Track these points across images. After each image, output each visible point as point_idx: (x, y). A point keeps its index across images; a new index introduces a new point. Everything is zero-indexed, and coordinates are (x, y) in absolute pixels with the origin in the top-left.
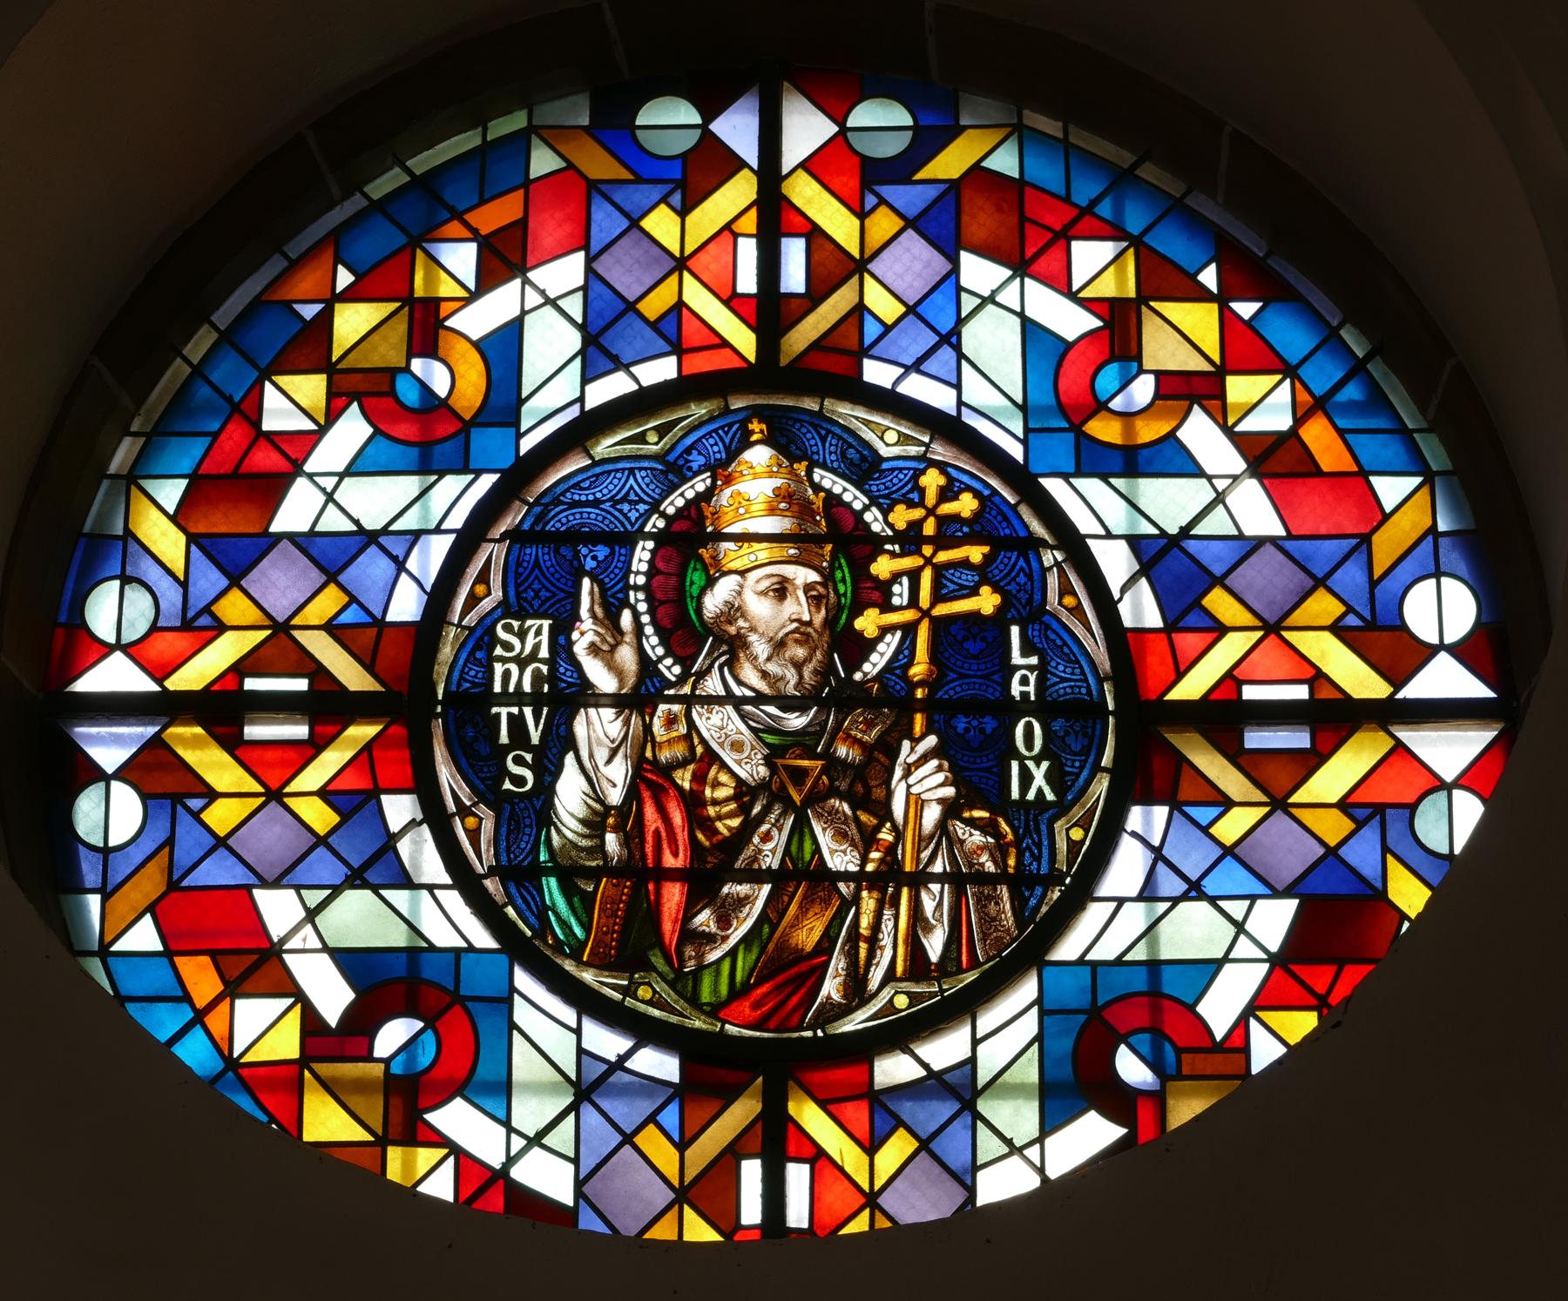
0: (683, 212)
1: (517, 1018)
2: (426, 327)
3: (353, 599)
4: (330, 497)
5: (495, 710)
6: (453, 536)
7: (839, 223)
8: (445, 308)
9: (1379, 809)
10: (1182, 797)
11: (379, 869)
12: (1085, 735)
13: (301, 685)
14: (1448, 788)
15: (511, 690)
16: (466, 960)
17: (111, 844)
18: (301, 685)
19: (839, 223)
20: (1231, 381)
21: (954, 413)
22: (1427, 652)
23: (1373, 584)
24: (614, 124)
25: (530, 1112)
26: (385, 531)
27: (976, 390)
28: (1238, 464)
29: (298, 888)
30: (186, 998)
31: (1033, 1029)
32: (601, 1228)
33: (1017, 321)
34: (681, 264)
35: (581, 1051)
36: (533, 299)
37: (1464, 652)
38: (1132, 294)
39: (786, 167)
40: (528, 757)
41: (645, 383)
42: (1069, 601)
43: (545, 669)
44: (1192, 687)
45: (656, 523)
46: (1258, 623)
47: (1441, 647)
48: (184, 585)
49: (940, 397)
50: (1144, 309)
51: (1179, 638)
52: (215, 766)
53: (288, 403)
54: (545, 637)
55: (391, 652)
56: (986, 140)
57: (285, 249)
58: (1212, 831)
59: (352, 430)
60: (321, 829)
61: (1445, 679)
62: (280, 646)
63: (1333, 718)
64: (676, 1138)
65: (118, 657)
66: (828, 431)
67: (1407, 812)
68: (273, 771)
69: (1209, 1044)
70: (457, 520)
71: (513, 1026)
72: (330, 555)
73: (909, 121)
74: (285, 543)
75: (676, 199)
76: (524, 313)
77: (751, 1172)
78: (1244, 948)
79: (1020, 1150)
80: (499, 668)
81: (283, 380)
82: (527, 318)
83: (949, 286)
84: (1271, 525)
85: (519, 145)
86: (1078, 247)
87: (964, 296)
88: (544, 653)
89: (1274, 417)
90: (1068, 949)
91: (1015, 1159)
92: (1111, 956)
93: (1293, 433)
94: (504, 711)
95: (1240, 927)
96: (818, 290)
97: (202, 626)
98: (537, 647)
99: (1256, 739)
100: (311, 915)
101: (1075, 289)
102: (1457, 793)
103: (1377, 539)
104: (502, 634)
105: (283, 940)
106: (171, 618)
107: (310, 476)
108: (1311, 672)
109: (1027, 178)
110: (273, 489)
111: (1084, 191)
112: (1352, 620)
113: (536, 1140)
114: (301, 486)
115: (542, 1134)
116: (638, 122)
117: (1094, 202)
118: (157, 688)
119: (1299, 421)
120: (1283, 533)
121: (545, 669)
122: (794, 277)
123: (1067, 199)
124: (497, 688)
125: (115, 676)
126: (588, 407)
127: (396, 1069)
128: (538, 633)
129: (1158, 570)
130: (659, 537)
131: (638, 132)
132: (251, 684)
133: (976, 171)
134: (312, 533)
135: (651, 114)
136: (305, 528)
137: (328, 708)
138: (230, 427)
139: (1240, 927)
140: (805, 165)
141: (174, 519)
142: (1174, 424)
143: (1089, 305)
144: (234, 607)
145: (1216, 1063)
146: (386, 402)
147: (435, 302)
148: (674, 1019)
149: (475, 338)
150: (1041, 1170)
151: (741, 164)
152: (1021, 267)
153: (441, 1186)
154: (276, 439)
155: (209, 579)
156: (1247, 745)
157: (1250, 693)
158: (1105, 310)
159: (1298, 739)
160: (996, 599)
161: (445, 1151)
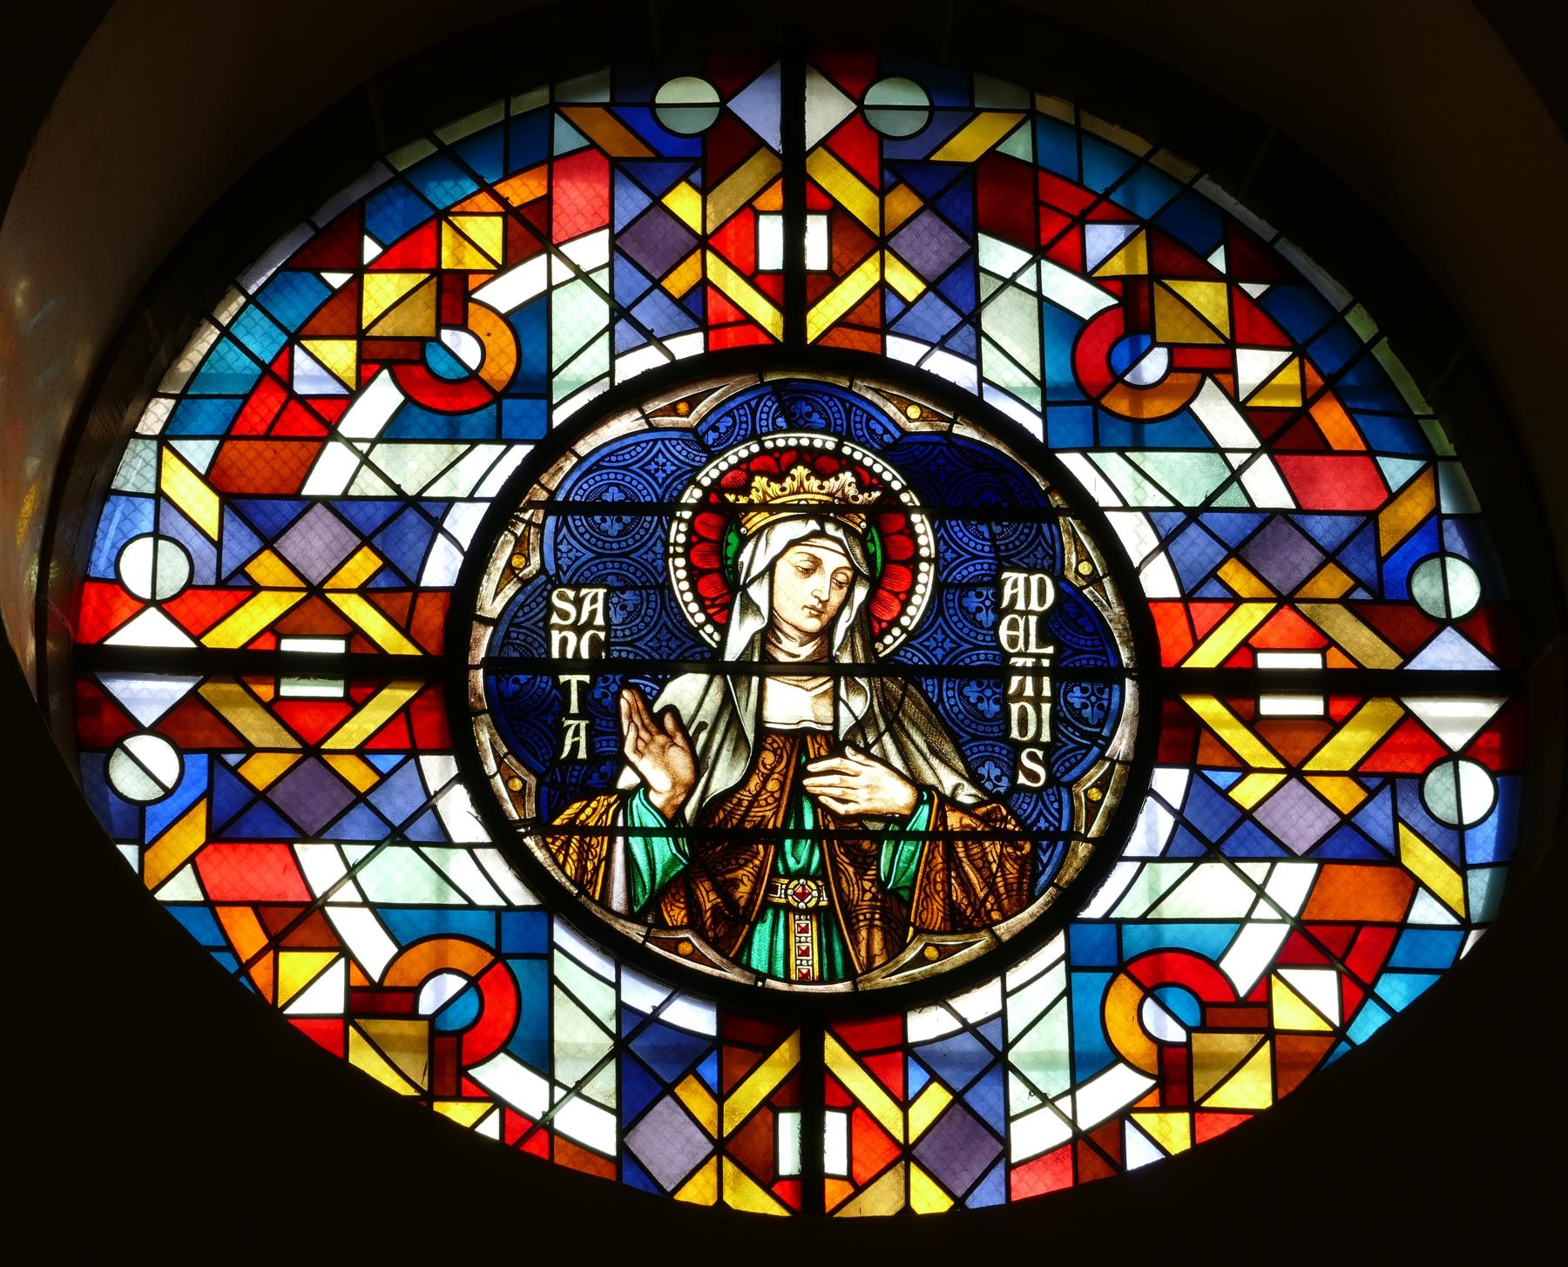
0: (704, 190)
1: (558, 972)
2: (453, 297)
5: (563, 678)
6: (487, 505)
7: (857, 199)
8: (473, 281)
9: (1390, 779)
10: (1200, 761)
12: (1101, 707)
19: (857, 199)
22: (1432, 626)
24: (634, 104)
28: (1250, 439)
33: (1033, 301)
34: (703, 242)
36: (561, 272)
40: (1040, 754)
41: (679, 357)
42: (682, 407)
43: (602, 635)
44: (1209, 655)
45: (692, 495)
46: (1271, 594)
48: (218, 545)
50: (1156, 286)
51: (1196, 608)
52: (253, 724)
53: (1310, 1000)
54: (600, 605)
55: (431, 616)
56: (1002, 124)
57: (313, 219)
60: (362, 787)
61: (149, 697)
62: (1293, 749)
63: (1347, 687)
64: (715, 1089)
65: (152, 612)
66: (852, 405)
67: (1416, 782)
69: (1232, 999)
71: (553, 980)
73: (925, 102)
74: (319, 508)
76: (551, 288)
77: (789, 1125)
78: (1263, 910)
80: (556, 636)
82: (555, 294)
84: (1283, 500)
85: (542, 121)
87: (983, 277)
88: (599, 620)
89: (295, 966)
91: (1046, 1110)
94: (574, 679)
95: (1260, 891)
96: (749, 213)
97: (237, 587)
98: (593, 614)
99: (1270, 706)
100: (352, 872)
102: (147, 596)
105: (326, 895)
106: (207, 575)
107: (349, 442)
109: (1041, 163)
111: (1098, 178)
112: (1361, 594)
113: (576, 1090)
114: (334, 450)
115: (580, 1084)
116: (658, 100)
117: (1109, 191)
119: (1309, 402)
121: (602, 635)
122: (816, 257)
123: (1079, 184)
125: (150, 631)
126: (618, 380)
128: (594, 600)
129: (1175, 548)
130: (697, 508)
131: (660, 113)
132: (288, 645)
133: (992, 155)
135: (668, 94)
136: (338, 492)
137: (364, 670)
138: (262, 393)
139: (1260, 891)
140: (823, 143)
141: (206, 479)
143: (1101, 283)
144: (266, 568)
145: (1242, 1015)
146: (418, 371)
147: (462, 275)
148: (716, 972)
149: (503, 311)
150: (1073, 1123)
151: (758, 143)
152: (1040, 252)
153: (491, 1129)
154: (309, 401)
155: (241, 542)
157: (1266, 661)
158: (1117, 287)
159: (1313, 706)
160: (757, 478)
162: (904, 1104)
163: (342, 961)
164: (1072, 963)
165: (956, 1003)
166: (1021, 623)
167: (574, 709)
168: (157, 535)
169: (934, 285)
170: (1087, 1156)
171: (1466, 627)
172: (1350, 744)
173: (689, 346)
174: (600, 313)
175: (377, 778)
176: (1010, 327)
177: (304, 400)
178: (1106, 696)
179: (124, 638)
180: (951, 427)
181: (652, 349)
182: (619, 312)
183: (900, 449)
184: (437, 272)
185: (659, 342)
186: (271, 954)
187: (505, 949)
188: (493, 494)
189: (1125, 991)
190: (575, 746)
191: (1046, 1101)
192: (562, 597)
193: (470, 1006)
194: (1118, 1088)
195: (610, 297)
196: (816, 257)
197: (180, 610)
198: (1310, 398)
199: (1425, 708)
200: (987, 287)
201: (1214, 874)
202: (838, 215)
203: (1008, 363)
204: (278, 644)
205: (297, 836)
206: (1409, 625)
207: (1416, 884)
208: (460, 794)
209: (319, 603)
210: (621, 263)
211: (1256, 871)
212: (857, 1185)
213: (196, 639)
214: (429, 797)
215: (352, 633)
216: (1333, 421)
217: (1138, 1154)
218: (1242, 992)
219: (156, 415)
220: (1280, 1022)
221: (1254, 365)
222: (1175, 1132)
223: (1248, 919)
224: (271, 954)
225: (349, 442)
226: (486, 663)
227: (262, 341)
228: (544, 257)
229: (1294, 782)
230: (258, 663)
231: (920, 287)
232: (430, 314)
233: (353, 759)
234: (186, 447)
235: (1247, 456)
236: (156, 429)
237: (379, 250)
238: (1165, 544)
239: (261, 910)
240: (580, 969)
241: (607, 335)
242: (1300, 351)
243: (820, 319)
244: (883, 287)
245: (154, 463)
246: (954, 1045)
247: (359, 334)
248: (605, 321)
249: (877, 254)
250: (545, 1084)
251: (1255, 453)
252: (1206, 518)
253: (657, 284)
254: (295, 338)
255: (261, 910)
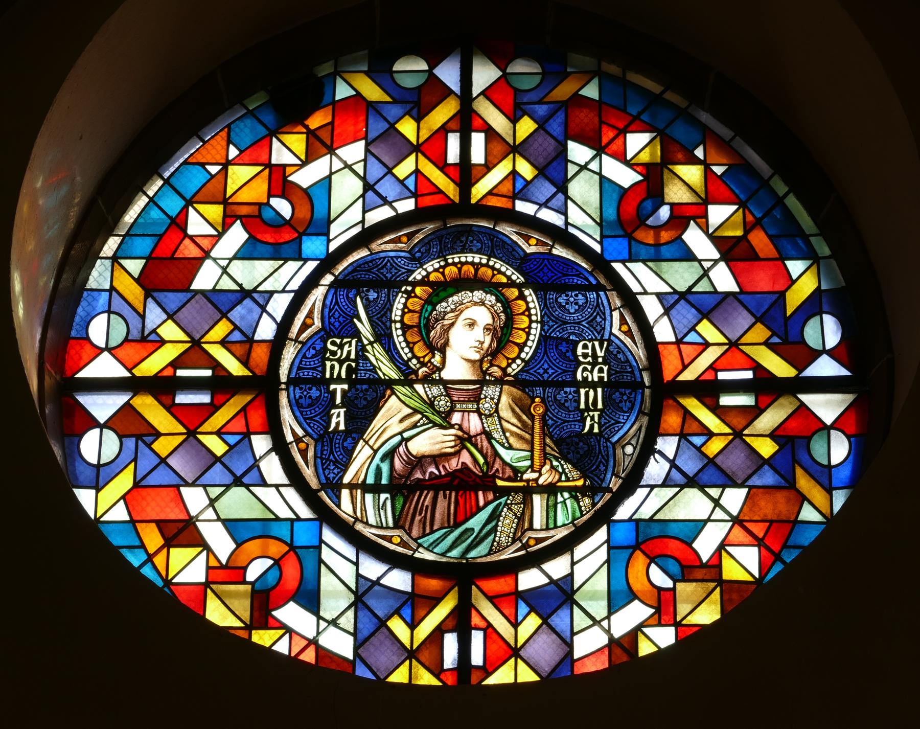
0: (418, 119)
1: (324, 557)
3: (699, 449)
4: (225, 270)
5: (332, 387)
6: (292, 294)
8: (289, 170)
9: (143, 339)
11: (247, 477)
13: (208, 373)
14: (108, 349)
15: (335, 377)
16: (626, 256)
17: (102, 462)
18: (208, 373)
20: (711, 208)
21: (564, 227)
22: (814, 355)
23: (135, 460)
25: (329, 608)
26: (255, 290)
27: (575, 215)
29: (205, 486)
30: (143, 546)
31: (604, 557)
32: (370, 676)
33: (597, 177)
35: (358, 575)
37: (91, 422)
38: (659, 161)
39: (475, 94)
41: (400, 212)
42: (625, 328)
47: (102, 427)
49: (555, 219)
53: (744, 563)
58: (703, 449)
59: (237, 235)
60: (219, 454)
61: (102, 406)
63: (766, 387)
65: (106, 354)
68: (192, 420)
70: (295, 285)
71: (321, 561)
72: (222, 302)
73: (540, 71)
75: (415, 112)
79: (599, 622)
80: (328, 364)
81: (749, 578)
83: (361, 637)
84: (733, 287)
86: (629, 137)
88: (353, 356)
89: (179, 556)
90: (624, 512)
91: (596, 628)
92: (290, 263)
93: (744, 238)
98: (349, 352)
99: (726, 400)
100: (212, 502)
101: (628, 158)
102: (103, 346)
103: (130, 484)
104: (330, 346)
105: (197, 516)
106: (135, 334)
107: (215, 260)
108: (172, 410)
110: (195, 265)
112: (776, 340)
116: (394, 69)
117: (640, 113)
118: (129, 375)
119: (747, 231)
120: (181, 488)
121: (353, 365)
124: (328, 376)
125: (105, 367)
127: (258, 586)
131: (395, 75)
134: (214, 290)
140: (484, 93)
142: (679, 232)
152: (600, 149)
153: (282, 647)
156: (721, 404)
158: (271, 621)
161: (283, 631)
162: (515, 625)
163: (205, 552)
164: (611, 546)
165: (545, 566)
166: (590, 345)
167: (338, 401)
168: (109, 312)
169: (542, 172)
170: (618, 651)
171: (833, 353)
172: (770, 419)
173: (408, 205)
174: (358, 186)
175: (227, 448)
176: (583, 189)
177: (192, 238)
178: (633, 396)
179: (87, 373)
180: (550, 250)
181: (387, 207)
182: (368, 187)
183: (522, 262)
184: (268, 165)
185: (390, 204)
186: (165, 550)
187: (297, 544)
188: (296, 288)
189: (640, 560)
190: (338, 424)
191: (596, 622)
192: (333, 343)
193: (275, 573)
194: (635, 613)
195: (363, 179)
196: (478, 155)
197: (120, 353)
198: (748, 228)
199: (808, 399)
200: (572, 170)
201: (693, 494)
202: (490, 133)
203: (582, 212)
204: (175, 372)
205: (182, 483)
206: (802, 355)
207: (803, 498)
208: (274, 458)
209: (197, 348)
210: (371, 160)
211: (714, 492)
212: (488, 668)
213: (130, 370)
214: (256, 460)
215: (215, 365)
216: (760, 240)
217: (645, 649)
218: (705, 560)
219: (111, 245)
220: (726, 575)
221: (718, 214)
222: (665, 637)
223: (709, 520)
224: (165, 550)
225: (215, 260)
226: (291, 381)
227: (173, 205)
228: (329, 156)
229: (737, 440)
230: (162, 387)
231: (390, 624)
232: (265, 187)
233: (215, 437)
234: (126, 263)
235: (712, 263)
236: (110, 254)
237: (237, 152)
238: (667, 312)
239: (161, 525)
240: (337, 554)
241: (361, 199)
242: (742, 205)
243: (479, 190)
244: (514, 174)
245: (110, 269)
246: (548, 588)
247: (225, 201)
248: (360, 191)
249: (517, 143)
250: (314, 619)
251: (716, 262)
252: (690, 297)
253: (390, 171)
254: (189, 202)
255: (161, 525)
